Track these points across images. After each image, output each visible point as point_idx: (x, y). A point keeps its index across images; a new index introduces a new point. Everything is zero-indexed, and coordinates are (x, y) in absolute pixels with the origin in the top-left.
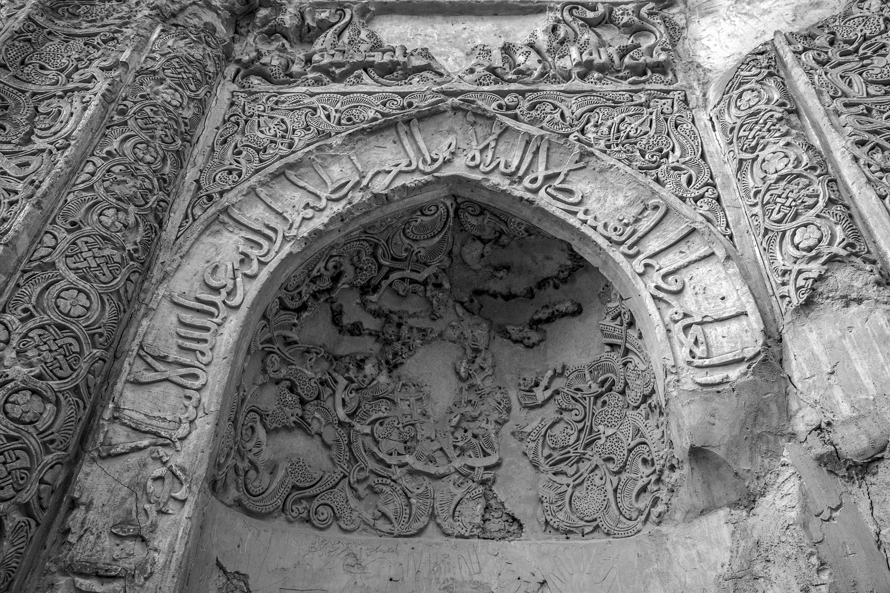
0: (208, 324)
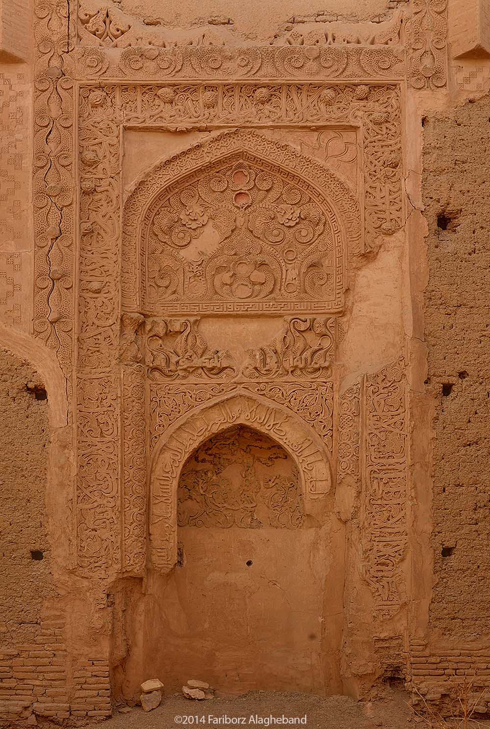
0: (168, 484)
